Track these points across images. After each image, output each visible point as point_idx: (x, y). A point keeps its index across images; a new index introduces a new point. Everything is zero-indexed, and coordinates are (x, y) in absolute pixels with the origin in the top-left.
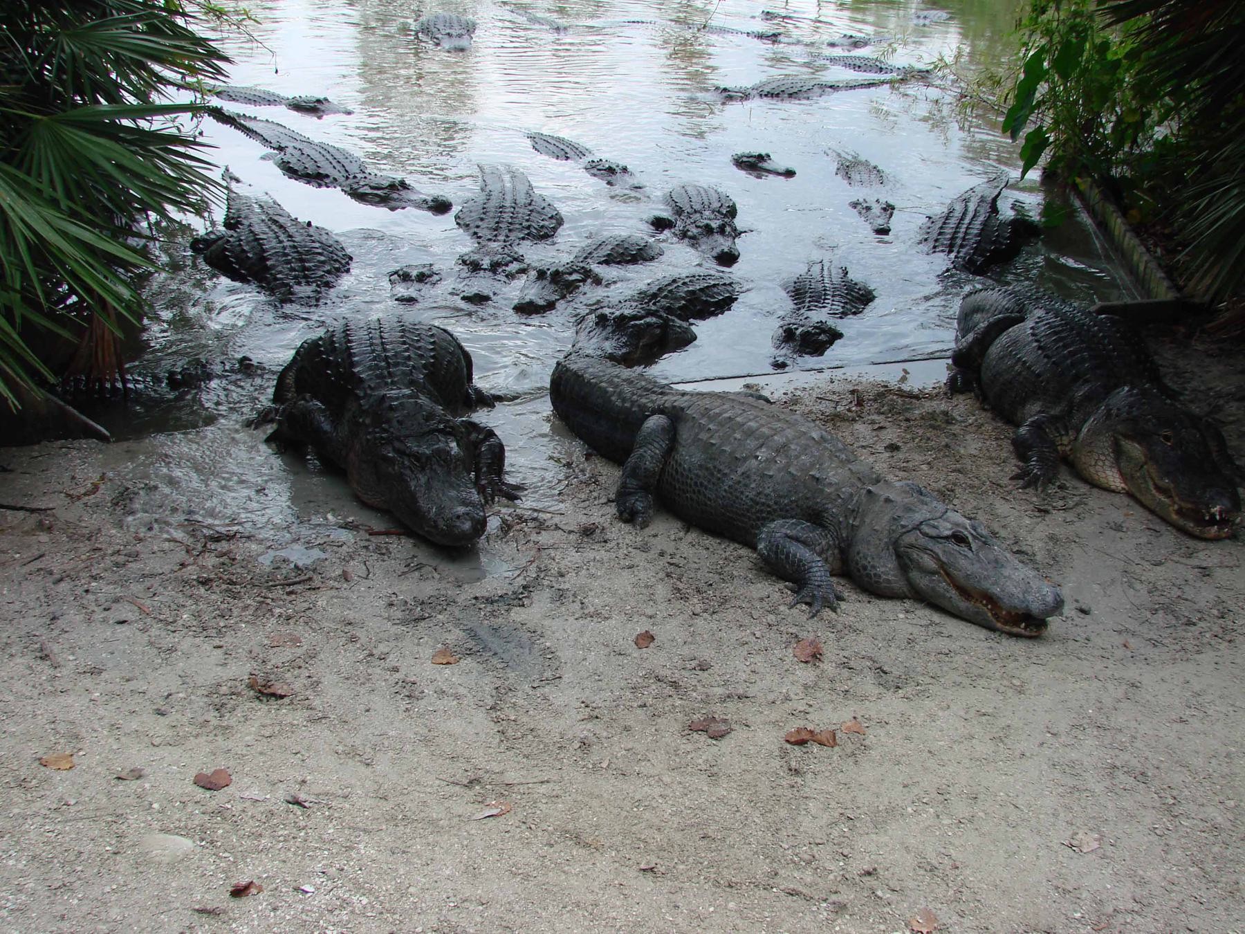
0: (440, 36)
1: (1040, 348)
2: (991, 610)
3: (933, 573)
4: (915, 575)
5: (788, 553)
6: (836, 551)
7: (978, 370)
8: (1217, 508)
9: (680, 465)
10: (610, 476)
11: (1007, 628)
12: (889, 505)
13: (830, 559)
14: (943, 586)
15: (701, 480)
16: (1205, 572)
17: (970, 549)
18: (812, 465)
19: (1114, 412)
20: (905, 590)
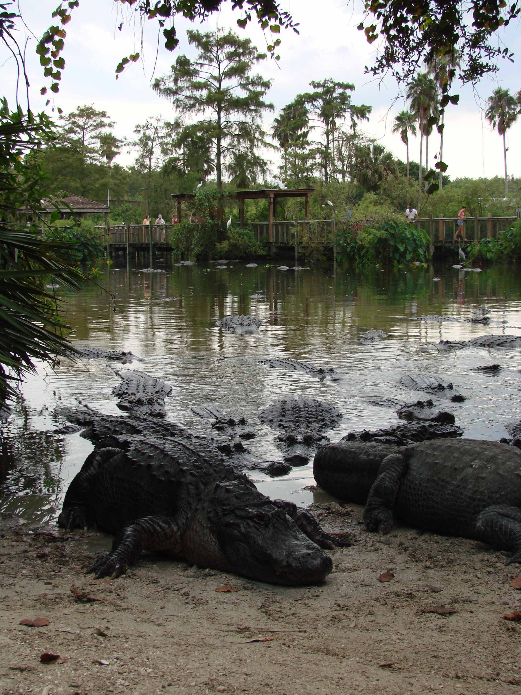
0: (235, 326)
9: (412, 482)
10: (358, 511)
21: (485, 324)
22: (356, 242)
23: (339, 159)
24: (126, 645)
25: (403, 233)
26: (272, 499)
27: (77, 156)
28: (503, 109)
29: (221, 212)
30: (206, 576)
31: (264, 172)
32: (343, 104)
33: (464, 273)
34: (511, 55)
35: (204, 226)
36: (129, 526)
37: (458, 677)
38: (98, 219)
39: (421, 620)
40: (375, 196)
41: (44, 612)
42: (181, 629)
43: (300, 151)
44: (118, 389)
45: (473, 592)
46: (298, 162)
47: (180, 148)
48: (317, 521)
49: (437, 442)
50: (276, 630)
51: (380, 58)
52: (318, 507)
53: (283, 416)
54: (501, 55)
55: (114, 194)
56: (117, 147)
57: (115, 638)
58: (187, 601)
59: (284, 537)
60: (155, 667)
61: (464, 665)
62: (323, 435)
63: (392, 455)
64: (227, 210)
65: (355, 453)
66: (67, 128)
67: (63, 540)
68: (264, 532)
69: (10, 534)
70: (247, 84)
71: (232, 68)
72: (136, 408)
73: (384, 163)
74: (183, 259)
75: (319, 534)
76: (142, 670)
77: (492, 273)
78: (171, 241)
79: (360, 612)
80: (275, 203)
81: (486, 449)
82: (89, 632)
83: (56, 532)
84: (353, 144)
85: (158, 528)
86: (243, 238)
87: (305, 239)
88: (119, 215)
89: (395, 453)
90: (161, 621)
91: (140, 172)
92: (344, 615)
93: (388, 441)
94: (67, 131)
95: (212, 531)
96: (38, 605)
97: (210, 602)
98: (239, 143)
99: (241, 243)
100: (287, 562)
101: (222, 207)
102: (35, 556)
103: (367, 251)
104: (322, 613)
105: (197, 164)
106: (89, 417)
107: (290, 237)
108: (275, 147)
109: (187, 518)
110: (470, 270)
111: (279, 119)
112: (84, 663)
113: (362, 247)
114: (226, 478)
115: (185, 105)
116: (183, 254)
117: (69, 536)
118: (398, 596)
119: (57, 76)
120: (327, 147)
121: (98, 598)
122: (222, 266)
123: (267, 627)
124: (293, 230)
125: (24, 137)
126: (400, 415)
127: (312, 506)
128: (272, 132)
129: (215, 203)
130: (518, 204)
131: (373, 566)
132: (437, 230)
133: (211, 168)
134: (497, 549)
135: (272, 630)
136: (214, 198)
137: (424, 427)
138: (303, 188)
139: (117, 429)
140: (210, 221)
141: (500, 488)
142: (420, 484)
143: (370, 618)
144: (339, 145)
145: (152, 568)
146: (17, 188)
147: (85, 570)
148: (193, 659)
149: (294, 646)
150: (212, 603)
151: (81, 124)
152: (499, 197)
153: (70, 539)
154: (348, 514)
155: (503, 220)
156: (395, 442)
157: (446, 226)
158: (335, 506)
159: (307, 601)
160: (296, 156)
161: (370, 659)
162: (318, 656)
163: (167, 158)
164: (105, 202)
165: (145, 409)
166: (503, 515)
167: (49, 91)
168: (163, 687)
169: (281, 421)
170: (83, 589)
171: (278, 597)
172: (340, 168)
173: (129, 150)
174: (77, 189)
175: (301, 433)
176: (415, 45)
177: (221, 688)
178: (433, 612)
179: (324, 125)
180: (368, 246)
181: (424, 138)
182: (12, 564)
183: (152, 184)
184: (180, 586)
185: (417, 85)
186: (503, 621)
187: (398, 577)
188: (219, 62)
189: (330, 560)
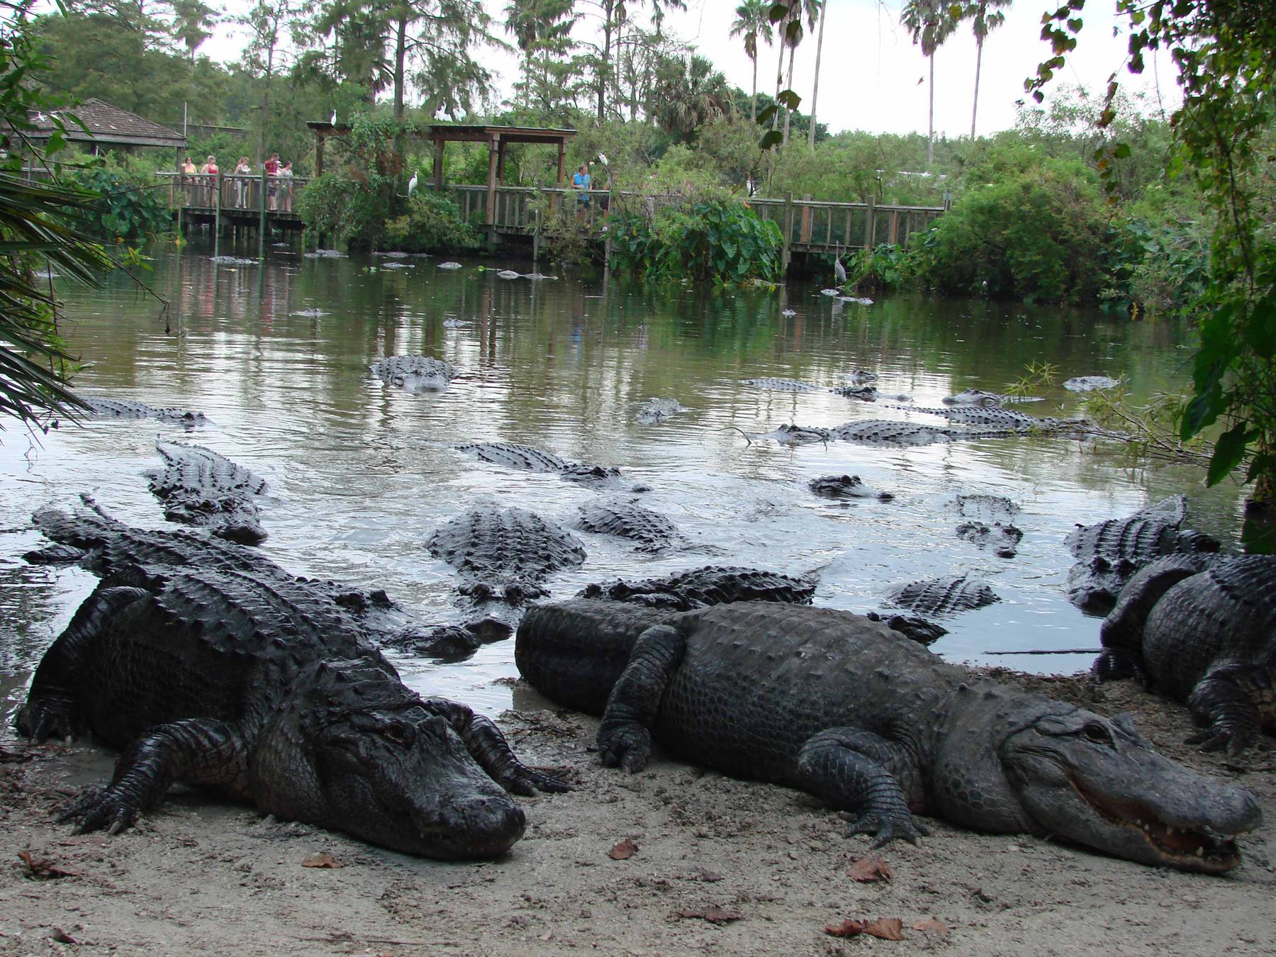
0: (404, 375)
1: (1223, 588)
2: (1150, 833)
3: (1058, 784)
4: (1032, 792)
6: (915, 773)
9: (690, 678)
10: (588, 728)
12: (991, 703)
14: (1073, 803)
15: (719, 694)
17: (1112, 747)
20: (1019, 817)
22: (648, 236)
23: (627, 79)
25: (735, 223)
27: (127, 33)
28: (933, 11)
29: (399, 161)
30: (290, 835)
33: (840, 306)
36: (149, 737)
38: (164, 159)
39: (676, 931)
40: (688, 152)
43: (555, 58)
45: (778, 884)
46: (551, 78)
48: (511, 744)
49: (741, 607)
50: (402, 940)
52: (516, 717)
53: (474, 545)
56: (209, 24)
57: (89, 947)
58: (244, 881)
59: (439, 769)
63: (657, 627)
64: (410, 158)
65: (592, 621)
67: (21, 759)
73: (709, 92)
74: (322, 246)
75: (509, 767)
77: (890, 307)
78: (302, 211)
79: (566, 913)
80: (501, 152)
81: (827, 625)
82: (40, 933)
84: (655, 53)
85: (206, 742)
86: (438, 214)
87: (553, 223)
89: (665, 623)
90: (186, 917)
92: (534, 917)
93: (660, 603)
95: (306, 753)
97: (288, 885)
98: (440, 32)
99: (432, 222)
100: (441, 815)
101: (401, 152)
103: (667, 254)
104: (494, 911)
105: (358, 67)
107: (525, 218)
109: (262, 726)
110: (852, 300)
113: (657, 245)
114: (339, 654)
117: (34, 752)
118: (641, 885)
120: (606, 55)
121: (71, 870)
122: (394, 264)
123: (387, 934)
124: (531, 205)
127: (506, 716)
128: (505, 17)
129: (390, 145)
130: (947, 185)
131: (603, 830)
132: (798, 223)
133: (384, 77)
134: (833, 807)
135: (395, 940)
136: (388, 135)
140: (377, 177)
142: (703, 684)
144: (628, 52)
145: (188, 818)
147: (56, 816)
152: (914, 170)
153: (35, 759)
154: (570, 733)
155: (918, 212)
156: (674, 605)
157: (816, 217)
158: (549, 717)
159: (470, 890)
160: (548, 66)
163: (301, 52)
164: (179, 128)
165: (219, 521)
166: (847, 746)
169: (469, 554)
170: (46, 854)
171: (418, 881)
172: (628, 94)
174: (124, 97)
178: (698, 917)
180: (668, 243)
181: (787, 50)
183: (272, 99)
186: (824, 936)
187: (644, 851)
189: (521, 815)
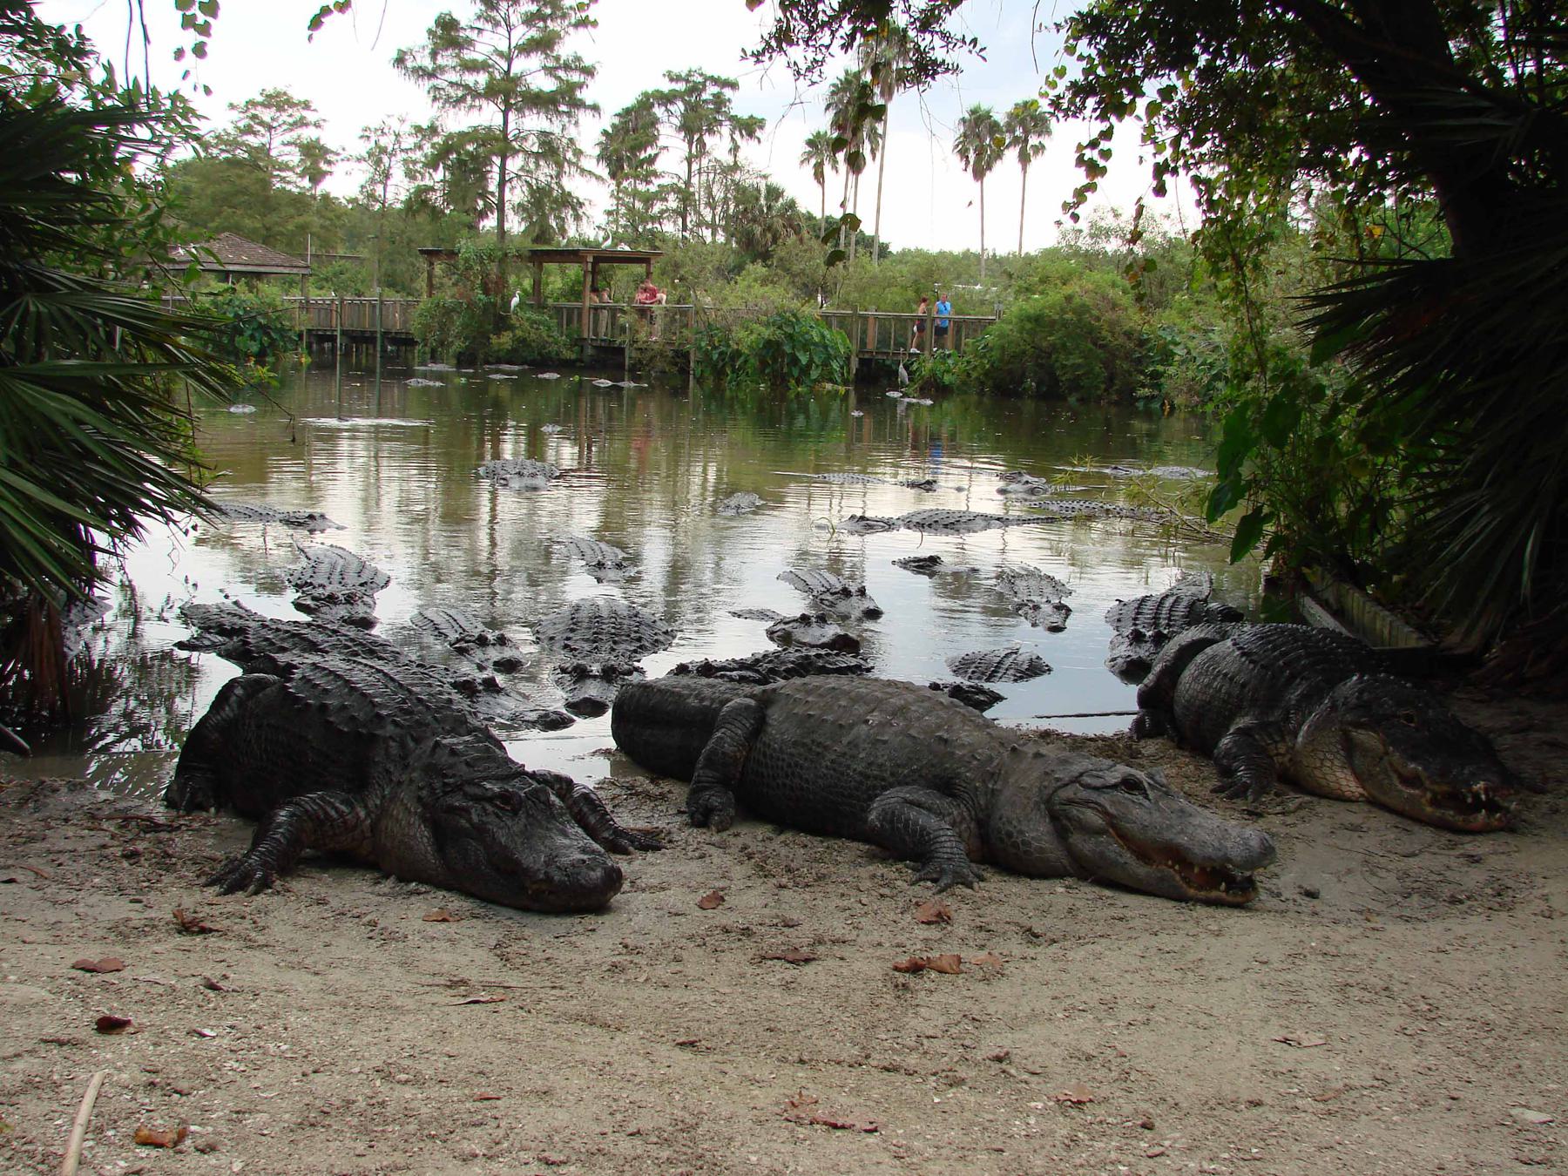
1: (1243, 654)
3: (1099, 832)
4: (1076, 839)
5: (907, 820)
6: (972, 825)
7: (1170, 708)
8: (1481, 785)
10: (678, 792)
11: (1202, 894)
13: (966, 835)
14: (1113, 849)
16: (1474, 860)
17: (1147, 797)
18: (939, 727)
19: (1340, 703)
21: (928, 491)
22: (729, 346)
23: (708, 204)
24: (253, 1006)
26: (529, 769)
28: (982, 140)
29: (502, 282)
30: (411, 893)
31: (577, 218)
32: (718, 112)
34: (982, 50)
35: (470, 305)
37: (802, 1061)
39: (758, 971)
41: (119, 948)
42: (352, 981)
43: (642, 187)
44: (297, 575)
46: (639, 205)
47: (436, 169)
48: (609, 808)
51: (766, 37)
53: (572, 630)
54: (967, 48)
55: (318, 242)
56: (329, 163)
58: (371, 934)
60: (295, 1041)
61: (816, 1042)
62: (636, 664)
63: (738, 700)
64: (512, 279)
65: (680, 695)
66: (241, 125)
67: (171, 828)
68: (509, 823)
69: (79, 817)
70: (556, 68)
71: (532, 40)
72: (324, 609)
73: (782, 216)
76: (271, 1046)
78: (415, 327)
79: (661, 958)
80: (594, 272)
82: (192, 982)
83: (159, 812)
85: (333, 813)
88: (326, 280)
89: (746, 696)
90: (320, 967)
91: (367, 209)
92: (631, 962)
93: (742, 679)
94: (241, 131)
95: (424, 820)
96: (112, 936)
98: (538, 166)
102: (119, 854)
103: (746, 361)
104: (596, 957)
105: (464, 199)
106: (240, 622)
107: (617, 332)
108: (599, 178)
109: (384, 797)
110: (914, 401)
111: (610, 131)
112: (173, 1033)
114: (454, 732)
115: (449, 97)
116: (433, 351)
118: (727, 932)
119: (205, 30)
120: (688, 183)
121: (218, 927)
123: (500, 979)
124: (623, 320)
125: (142, 132)
126: (771, 634)
128: (597, 151)
129: (493, 268)
132: (864, 332)
134: (901, 859)
137: (807, 657)
138: (643, 249)
139: (285, 645)
140: (482, 297)
141: (910, 759)
143: (675, 967)
145: (320, 880)
146: (124, 221)
147: (203, 880)
148: (363, 1029)
149: (538, 1012)
150: (414, 939)
151: (267, 119)
153: (184, 828)
154: (662, 797)
155: (973, 322)
157: (880, 327)
158: (643, 782)
159: (574, 939)
160: (635, 194)
161: (662, 1033)
162: (577, 1028)
163: (412, 186)
164: (303, 257)
165: (342, 611)
166: (912, 803)
167: (190, 56)
168: (304, 1075)
171: (527, 932)
172: (709, 218)
173: (349, 169)
174: (255, 231)
175: (598, 661)
176: (826, 19)
177: (403, 1077)
178: (778, 958)
179: (685, 146)
181: (852, 177)
182: (77, 867)
183: (387, 229)
184: (364, 910)
185: (844, 90)
186: (891, 973)
188: (510, 28)
